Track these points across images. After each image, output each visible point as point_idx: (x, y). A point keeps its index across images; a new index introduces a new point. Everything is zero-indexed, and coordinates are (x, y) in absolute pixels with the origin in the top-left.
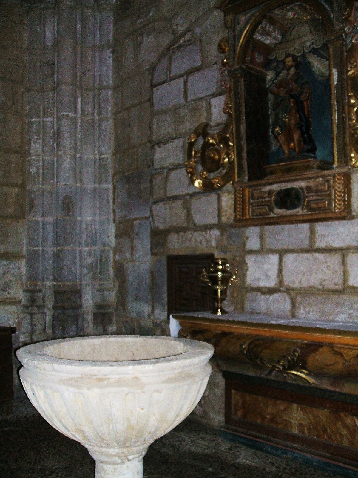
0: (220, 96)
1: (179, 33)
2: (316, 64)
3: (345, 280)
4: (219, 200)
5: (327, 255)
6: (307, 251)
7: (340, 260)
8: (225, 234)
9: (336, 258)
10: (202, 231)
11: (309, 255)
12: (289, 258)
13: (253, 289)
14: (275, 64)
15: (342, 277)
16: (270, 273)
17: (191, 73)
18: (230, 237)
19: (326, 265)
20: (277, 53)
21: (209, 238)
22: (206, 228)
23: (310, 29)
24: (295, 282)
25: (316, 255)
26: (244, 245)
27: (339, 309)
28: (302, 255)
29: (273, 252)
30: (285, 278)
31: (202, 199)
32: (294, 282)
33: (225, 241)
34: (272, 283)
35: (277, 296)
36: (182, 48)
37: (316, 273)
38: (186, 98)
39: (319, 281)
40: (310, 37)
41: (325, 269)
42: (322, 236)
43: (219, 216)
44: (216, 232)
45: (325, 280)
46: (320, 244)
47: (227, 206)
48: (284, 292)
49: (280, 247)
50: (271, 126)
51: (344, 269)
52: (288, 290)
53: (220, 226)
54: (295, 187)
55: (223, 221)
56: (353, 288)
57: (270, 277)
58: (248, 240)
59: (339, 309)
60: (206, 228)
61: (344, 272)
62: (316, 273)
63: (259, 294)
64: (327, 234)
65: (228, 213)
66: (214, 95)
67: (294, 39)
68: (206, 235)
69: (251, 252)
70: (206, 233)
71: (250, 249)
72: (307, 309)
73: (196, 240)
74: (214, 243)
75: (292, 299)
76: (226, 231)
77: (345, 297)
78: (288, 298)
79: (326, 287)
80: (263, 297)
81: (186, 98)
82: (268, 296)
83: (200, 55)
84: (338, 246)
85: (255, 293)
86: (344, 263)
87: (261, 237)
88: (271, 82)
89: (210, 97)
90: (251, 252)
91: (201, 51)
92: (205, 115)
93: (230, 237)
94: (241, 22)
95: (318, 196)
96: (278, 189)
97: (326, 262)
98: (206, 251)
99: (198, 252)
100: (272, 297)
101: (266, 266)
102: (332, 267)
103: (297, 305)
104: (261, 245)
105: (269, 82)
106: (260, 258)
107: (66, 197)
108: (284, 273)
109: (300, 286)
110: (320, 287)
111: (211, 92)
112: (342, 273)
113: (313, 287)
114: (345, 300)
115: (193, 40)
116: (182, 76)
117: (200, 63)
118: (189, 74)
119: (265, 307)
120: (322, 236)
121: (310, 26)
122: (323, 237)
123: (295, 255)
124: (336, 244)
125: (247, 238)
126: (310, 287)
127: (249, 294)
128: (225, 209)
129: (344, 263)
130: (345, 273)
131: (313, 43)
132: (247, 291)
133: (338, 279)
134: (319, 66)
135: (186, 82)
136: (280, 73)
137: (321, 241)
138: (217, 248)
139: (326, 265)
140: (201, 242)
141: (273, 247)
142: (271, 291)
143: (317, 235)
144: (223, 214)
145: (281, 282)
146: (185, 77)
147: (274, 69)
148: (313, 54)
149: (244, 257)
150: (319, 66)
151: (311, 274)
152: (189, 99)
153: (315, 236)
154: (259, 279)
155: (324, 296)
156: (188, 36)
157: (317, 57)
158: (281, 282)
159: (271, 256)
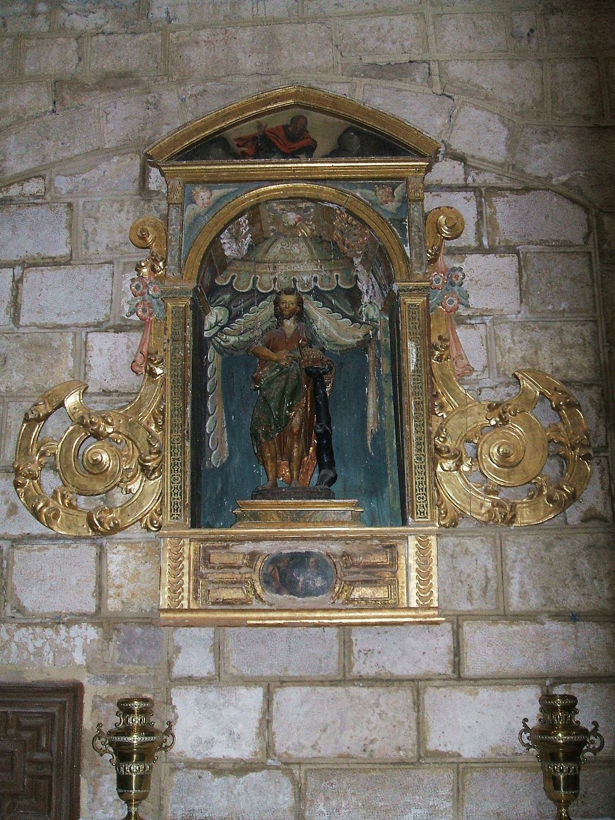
0: (116, 332)
1: (9, 174)
2: (320, 318)
3: (421, 740)
4: (101, 556)
5: (381, 690)
6: (333, 683)
7: (410, 701)
8: (115, 638)
9: (404, 696)
10: (45, 626)
11: (340, 690)
12: (289, 697)
13: (191, 765)
14: (227, 297)
15: (414, 734)
16: (238, 729)
17: (36, 265)
18: (128, 644)
19: (377, 710)
20: (233, 277)
21: (65, 645)
22: (57, 621)
23: (312, 253)
24: (303, 747)
25: (354, 690)
26: (170, 664)
27: (408, 799)
28: (320, 689)
29: (249, 682)
30: (278, 739)
31: (49, 553)
32: (301, 746)
33: (113, 652)
34: (245, 750)
35: (255, 777)
36: (13, 208)
37: (354, 728)
38: (16, 319)
39: (362, 743)
40: (310, 267)
41: (375, 718)
42: (368, 652)
43: (100, 593)
44: (92, 633)
45: (372, 742)
46: (362, 667)
47: (123, 575)
48: (278, 768)
49: (267, 673)
50: (210, 415)
51: (418, 718)
52: (287, 766)
53: (98, 618)
54: (316, 550)
55: (109, 608)
56: (438, 754)
57: (239, 737)
58: (180, 655)
59: (408, 799)
60: (57, 621)
61: (418, 723)
62: (354, 728)
63: (208, 775)
64: (377, 648)
65: (124, 590)
66: (99, 327)
67: (275, 261)
68: (54, 637)
69: (190, 681)
70: (57, 632)
71: (185, 674)
72: (334, 803)
73: (22, 647)
74: (79, 658)
75: (295, 782)
76: (118, 630)
77: (420, 773)
78: (285, 783)
79: (377, 755)
80: (218, 781)
81: (16, 319)
82: (231, 779)
83: (65, 234)
84: (405, 673)
85: (196, 772)
86: (418, 705)
87: (218, 650)
88: (217, 328)
89: (88, 330)
90: (190, 681)
91: (70, 227)
92: (71, 364)
93: (128, 644)
94: (199, 202)
95: (369, 573)
96: (274, 552)
97: (377, 705)
98: (59, 675)
99: (32, 676)
100: (241, 780)
101: (230, 713)
102: (390, 714)
103: (309, 796)
104: (218, 667)
105: (211, 328)
106: (212, 695)
107: (582, 521)
108: (275, 725)
109: (315, 754)
110: (365, 755)
111: (91, 320)
112: (414, 725)
113: (348, 756)
114: (420, 780)
115: (48, 197)
116: (11, 265)
117: (64, 251)
118: (29, 267)
119: (224, 802)
120: (368, 652)
121: (310, 248)
122: (369, 654)
123: (305, 689)
124: (402, 669)
125: (178, 650)
126: (341, 756)
127: (178, 777)
128: (118, 582)
129: (418, 705)
130: (420, 726)
131: (315, 279)
132: (174, 769)
133: (407, 739)
134: (327, 323)
135: (17, 283)
136: (239, 316)
137: (364, 663)
138: (88, 668)
139: (377, 710)
140: (38, 652)
141: (247, 672)
142: (241, 768)
143: (355, 649)
144: (111, 592)
145: (269, 748)
146: (18, 270)
147: (227, 306)
148: (315, 299)
149: (168, 690)
150: (327, 323)
151: (342, 729)
152: (23, 321)
153: (351, 652)
154: (210, 743)
155: (374, 773)
156: (33, 187)
157: (323, 306)
158: (269, 748)
159: (242, 690)
